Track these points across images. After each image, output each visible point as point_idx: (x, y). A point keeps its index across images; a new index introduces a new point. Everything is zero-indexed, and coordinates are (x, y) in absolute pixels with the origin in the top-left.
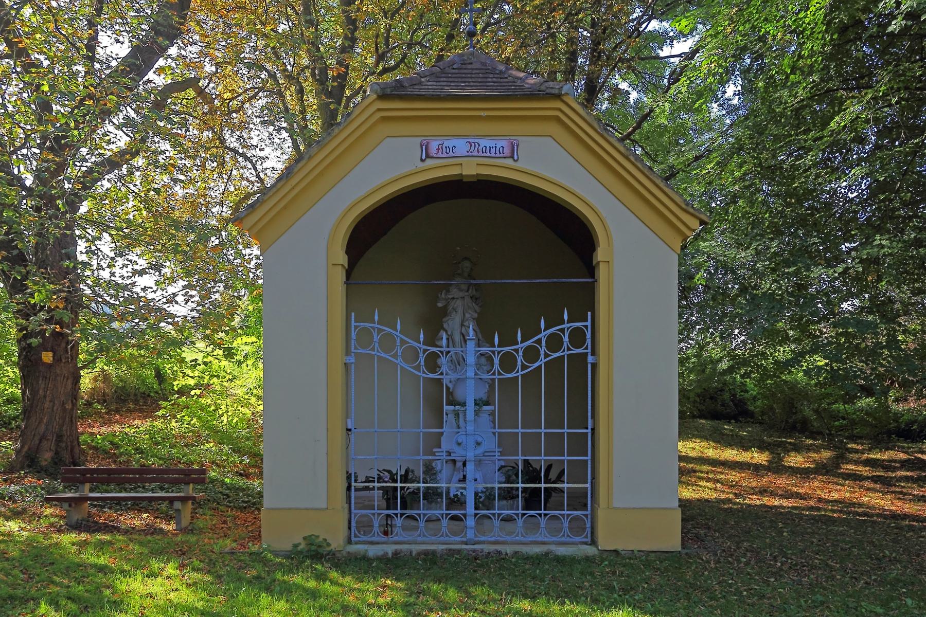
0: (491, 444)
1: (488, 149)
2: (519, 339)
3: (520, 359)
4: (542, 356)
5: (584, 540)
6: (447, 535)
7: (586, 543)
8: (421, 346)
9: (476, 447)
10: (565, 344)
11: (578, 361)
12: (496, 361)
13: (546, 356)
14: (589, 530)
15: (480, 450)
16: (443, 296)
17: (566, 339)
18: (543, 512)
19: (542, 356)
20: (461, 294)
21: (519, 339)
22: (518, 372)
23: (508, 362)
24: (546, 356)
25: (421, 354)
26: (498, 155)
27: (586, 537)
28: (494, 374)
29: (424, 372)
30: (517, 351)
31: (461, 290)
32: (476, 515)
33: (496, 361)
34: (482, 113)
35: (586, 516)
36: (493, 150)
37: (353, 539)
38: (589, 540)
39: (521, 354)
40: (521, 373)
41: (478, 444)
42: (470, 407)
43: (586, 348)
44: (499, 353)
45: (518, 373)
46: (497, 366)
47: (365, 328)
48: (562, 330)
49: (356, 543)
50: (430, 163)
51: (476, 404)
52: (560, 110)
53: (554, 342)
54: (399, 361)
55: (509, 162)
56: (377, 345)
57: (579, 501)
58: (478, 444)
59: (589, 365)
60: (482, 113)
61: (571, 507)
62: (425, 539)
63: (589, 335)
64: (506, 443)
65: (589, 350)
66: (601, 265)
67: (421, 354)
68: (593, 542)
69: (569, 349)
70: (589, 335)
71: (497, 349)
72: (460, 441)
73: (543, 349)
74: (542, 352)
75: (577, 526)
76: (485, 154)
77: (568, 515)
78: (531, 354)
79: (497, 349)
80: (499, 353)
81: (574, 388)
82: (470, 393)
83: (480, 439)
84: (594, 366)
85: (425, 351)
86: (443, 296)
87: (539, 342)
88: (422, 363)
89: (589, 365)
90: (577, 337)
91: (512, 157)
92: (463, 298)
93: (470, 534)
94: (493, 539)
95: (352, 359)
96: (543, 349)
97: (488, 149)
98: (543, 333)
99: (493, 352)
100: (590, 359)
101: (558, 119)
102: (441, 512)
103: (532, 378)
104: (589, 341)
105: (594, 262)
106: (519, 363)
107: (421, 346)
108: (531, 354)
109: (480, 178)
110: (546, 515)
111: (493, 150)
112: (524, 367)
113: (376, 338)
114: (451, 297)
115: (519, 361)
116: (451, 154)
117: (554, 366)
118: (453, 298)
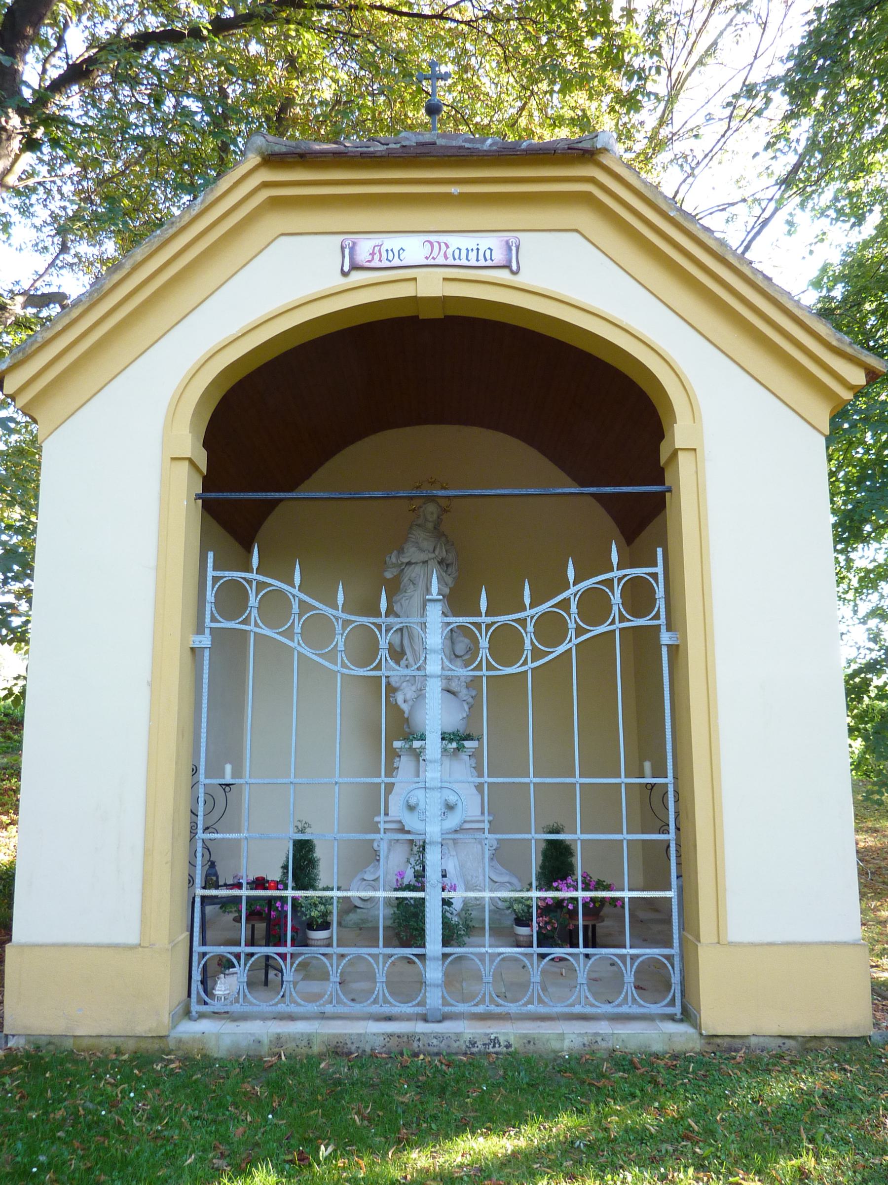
0: (471, 807)
1: (464, 253)
2: (527, 601)
3: (529, 639)
4: (572, 632)
5: (670, 1010)
6: (386, 1001)
7: (672, 1018)
8: (339, 613)
9: (452, 823)
10: (615, 609)
11: (642, 643)
12: (484, 643)
13: (579, 631)
14: (676, 988)
15: (453, 821)
16: (394, 560)
17: (616, 598)
18: (288, 949)
19: (572, 632)
20: (423, 557)
21: (527, 601)
22: (525, 663)
23: (506, 644)
24: (579, 631)
25: (339, 628)
26: (482, 263)
27: (672, 1003)
28: (479, 668)
29: (344, 665)
30: (523, 622)
31: (422, 550)
32: (445, 956)
33: (484, 643)
34: (455, 190)
35: (669, 958)
36: (472, 256)
37: (195, 1008)
38: (677, 1010)
39: (530, 628)
40: (531, 665)
41: (450, 807)
42: (433, 746)
43: (657, 617)
44: (488, 626)
45: (525, 666)
46: (484, 653)
47: (233, 582)
48: (609, 583)
49: (202, 1016)
50: (358, 277)
51: (443, 739)
52: (592, 180)
53: (594, 606)
54: (297, 644)
55: (503, 275)
56: (255, 613)
57: (653, 923)
58: (450, 807)
59: (664, 650)
60: (455, 190)
61: (642, 940)
62: (341, 1009)
63: (660, 592)
64: (502, 808)
65: (662, 621)
66: (681, 456)
67: (339, 628)
68: (688, 1015)
69: (622, 619)
70: (660, 592)
71: (484, 619)
72: (413, 801)
73: (573, 620)
74: (572, 625)
75: (652, 981)
76: (457, 262)
77: (634, 958)
78: (551, 629)
79: (484, 619)
80: (488, 626)
81: (642, 687)
82: (436, 715)
83: (452, 799)
84: (675, 650)
85: (346, 623)
86: (394, 560)
87: (565, 604)
88: (341, 647)
89: (664, 650)
90: (639, 596)
91: (508, 266)
92: (425, 562)
93: (434, 999)
94: (481, 1009)
95: (205, 641)
96: (573, 620)
97: (464, 253)
98: (573, 590)
99: (478, 625)
100: (666, 638)
101: (587, 199)
102: (236, 949)
103: (553, 675)
104: (661, 604)
105: (663, 460)
106: (528, 645)
107: (339, 613)
108: (551, 629)
109: (451, 312)
110: (542, 956)
111: (472, 256)
112: (537, 654)
113: (253, 601)
114: (406, 560)
115: (527, 642)
116: (396, 262)
117: (595, 651)
118: (409, 563)
